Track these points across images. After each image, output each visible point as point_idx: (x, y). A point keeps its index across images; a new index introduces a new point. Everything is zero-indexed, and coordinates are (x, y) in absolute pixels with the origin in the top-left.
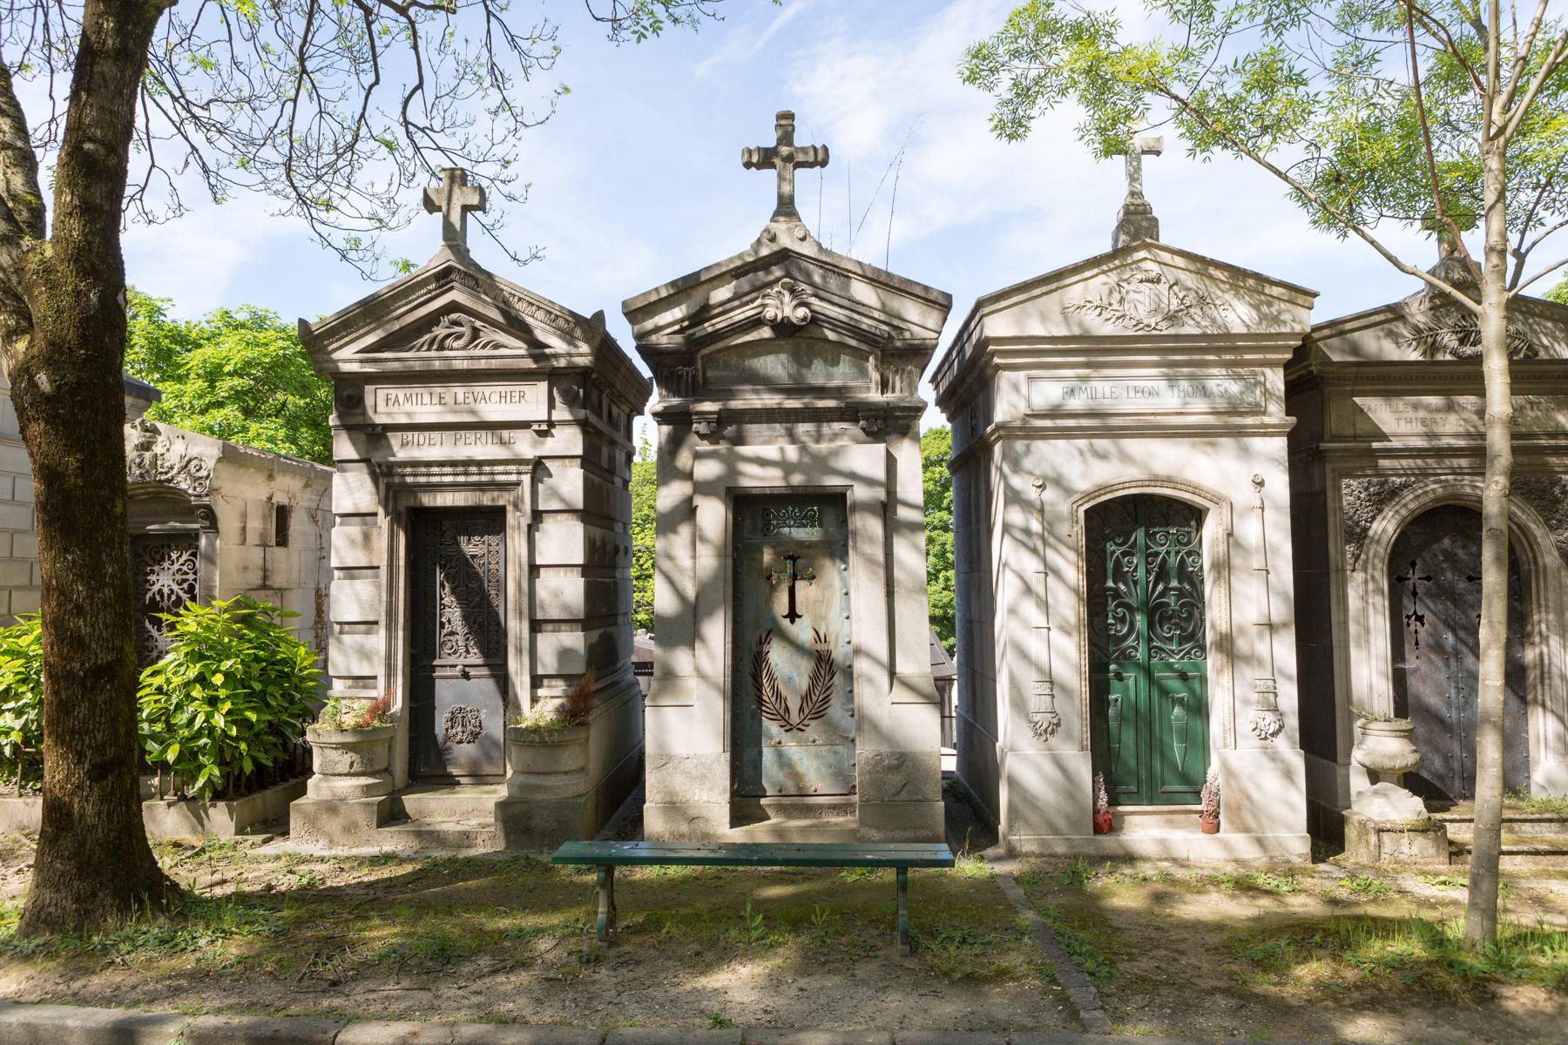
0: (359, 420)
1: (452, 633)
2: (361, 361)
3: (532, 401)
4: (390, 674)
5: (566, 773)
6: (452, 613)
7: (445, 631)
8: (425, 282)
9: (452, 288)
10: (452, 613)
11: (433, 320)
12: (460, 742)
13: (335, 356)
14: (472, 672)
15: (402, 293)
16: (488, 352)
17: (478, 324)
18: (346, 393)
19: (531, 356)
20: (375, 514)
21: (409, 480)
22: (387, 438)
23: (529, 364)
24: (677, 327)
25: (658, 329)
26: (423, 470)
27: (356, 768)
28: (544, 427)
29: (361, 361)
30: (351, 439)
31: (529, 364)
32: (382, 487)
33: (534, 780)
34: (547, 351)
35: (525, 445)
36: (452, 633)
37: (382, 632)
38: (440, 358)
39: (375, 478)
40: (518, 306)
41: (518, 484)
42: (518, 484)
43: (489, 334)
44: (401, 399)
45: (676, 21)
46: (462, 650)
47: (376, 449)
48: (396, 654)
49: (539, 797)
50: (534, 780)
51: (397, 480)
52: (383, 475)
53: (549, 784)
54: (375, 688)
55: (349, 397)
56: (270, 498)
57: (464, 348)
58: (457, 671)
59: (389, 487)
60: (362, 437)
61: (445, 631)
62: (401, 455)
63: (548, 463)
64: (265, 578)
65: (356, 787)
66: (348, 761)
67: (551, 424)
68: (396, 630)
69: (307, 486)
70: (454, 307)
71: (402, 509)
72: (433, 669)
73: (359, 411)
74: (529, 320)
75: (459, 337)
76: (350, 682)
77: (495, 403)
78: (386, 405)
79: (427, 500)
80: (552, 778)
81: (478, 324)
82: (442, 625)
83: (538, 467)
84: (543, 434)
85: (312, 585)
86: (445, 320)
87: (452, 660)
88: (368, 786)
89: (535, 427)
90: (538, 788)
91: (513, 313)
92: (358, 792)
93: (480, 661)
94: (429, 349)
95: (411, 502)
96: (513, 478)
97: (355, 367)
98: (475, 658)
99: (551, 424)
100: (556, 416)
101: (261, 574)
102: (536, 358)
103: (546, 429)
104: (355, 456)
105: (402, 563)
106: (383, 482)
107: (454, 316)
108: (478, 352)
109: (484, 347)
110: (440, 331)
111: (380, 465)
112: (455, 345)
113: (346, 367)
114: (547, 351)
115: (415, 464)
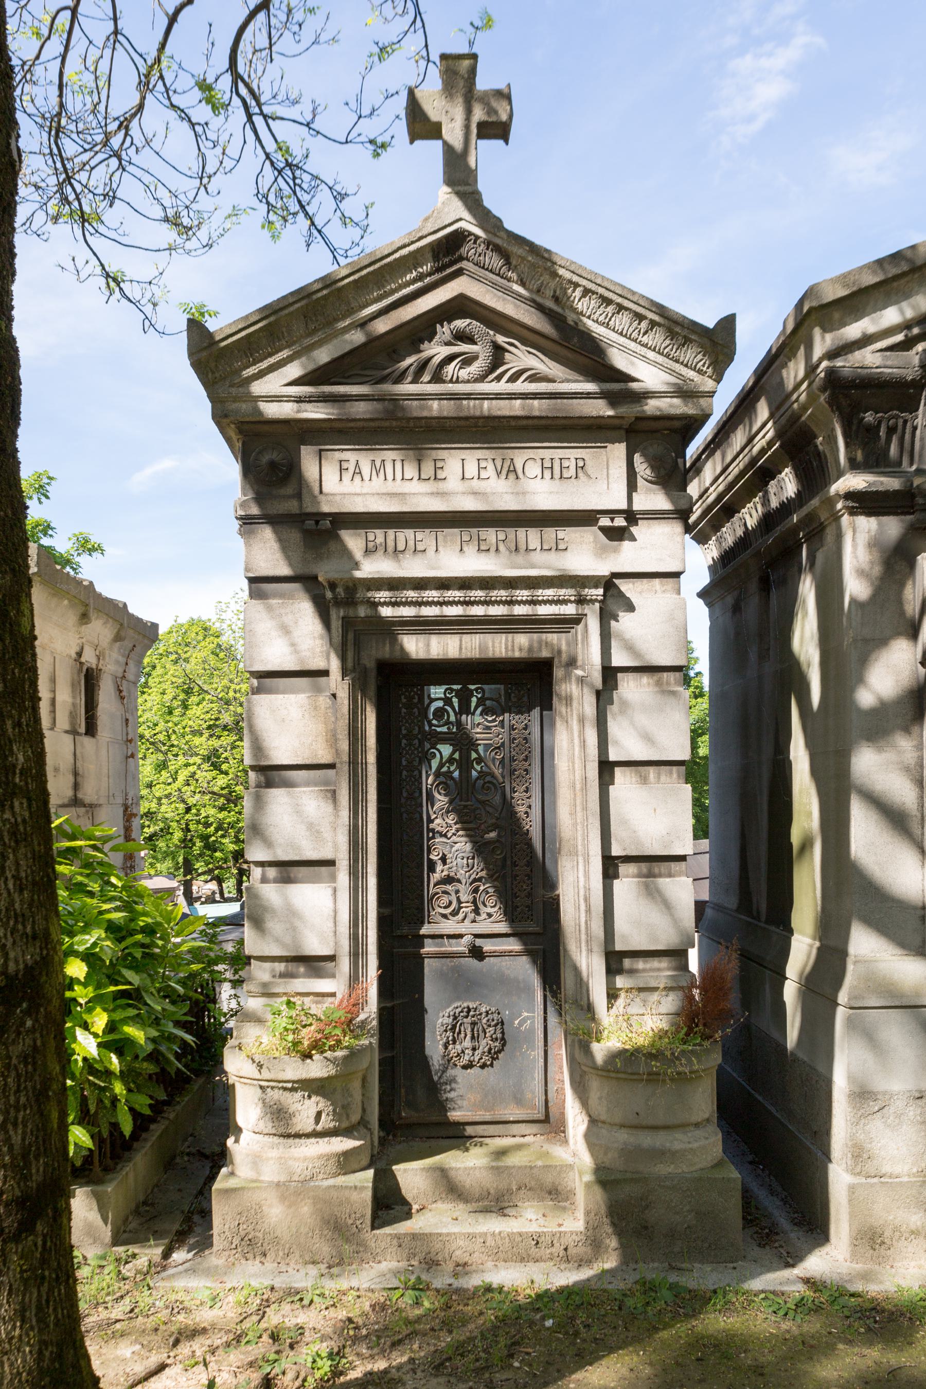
0: (292, 506)
1: (449, 880)
2: (299, 400)
3: (604, 478)
4: (357, 953)
5: (697, 1125)
6: (452, 850)
7: (436, 877)
8: (413, 260)
9: (459, 273)
10: (452, 850)
11: (422, 330)
12: (469, 1066)
13: (258, 388)
14: (488, 946)
15: (379, 275)
16: (520, 386)
17: (501, 339)
18: (266, 458)
19: (603, 395)
20: (325, 673)
21: (386, 612)
22: (338, 538)
23: (601, 409)
24: (900, 337)
25: (866, 340)
26: (411, 594)
27: (326, 1122)
28: (620, 522)
29: (299, 400)
30: (280, 540)
31: (601, 409)
32: (336, 624)
33: (647, 1140)
34: (634, 385)
35: (583, 555)
36: (449, 880)
37: (343, 878)
38: (440, 397)
39: (323, 611)
40: (582, 305)
41: (576, 620)
42: (576, 620)
43: (522, 357)
44: (366, 469)
45: (383, 51)
46: (467, 909)
47: (319, 557)
48: (365, 917)
49: (664, 1169)
50: (647, 1140)
51: (362, 612)
52: (338, 603)
53: (677, 1146)
54: (333, 976)
55: (273, 465)
56: (79, 654)
57: (481, 378)
58: (461, 946)
59: (347, 623)
60: (295, 536)
61: (436, 877)
62: (371, 568)
63: (626, 587)
64: (76, 786)
65: (328, 1157)
66: (312, 1113)
67: (632, 516)
68: (365, 876)
69: (118, 638)
70: (461, 307)
71: (370, 664)
72: (420, 940)
73: (289, 490)
74: (598, 330)
75: (468, 361)
76: (281, 967)
77: (537, 480)
78: (347, 481)
79: (415, 646)
80: (679, 1135)
81: (501, 339)
82: (432, 867)
83: (611, 594)
84: (617, 535)
85: (120, 800)
86: (445, 331)
87: (449, 926)
88: (346, 1154)
89: (605, 522)
90: (660, 1154)
91: (571, 317)
92: (332, 1167)
93: (503, 928)
94: (415, 381)
95: (385, 652)
96: (570, 610)
97: (285, 410)
98: (491, 919)
99: (632, 516)
100: (641, 502)
101: (71, 778)
102: (613, 399)
103: (620, 528)
104: (284, 570)
105: (372, 758)
106: (336, 616)
107: (460, 324)
108: (502, 386)
109: (513, 379)
110: (437, 350)
111: (333, 586)
112: (464, 374)
113: (272, 410)
114: (634, 385)
115: (395, 584)
